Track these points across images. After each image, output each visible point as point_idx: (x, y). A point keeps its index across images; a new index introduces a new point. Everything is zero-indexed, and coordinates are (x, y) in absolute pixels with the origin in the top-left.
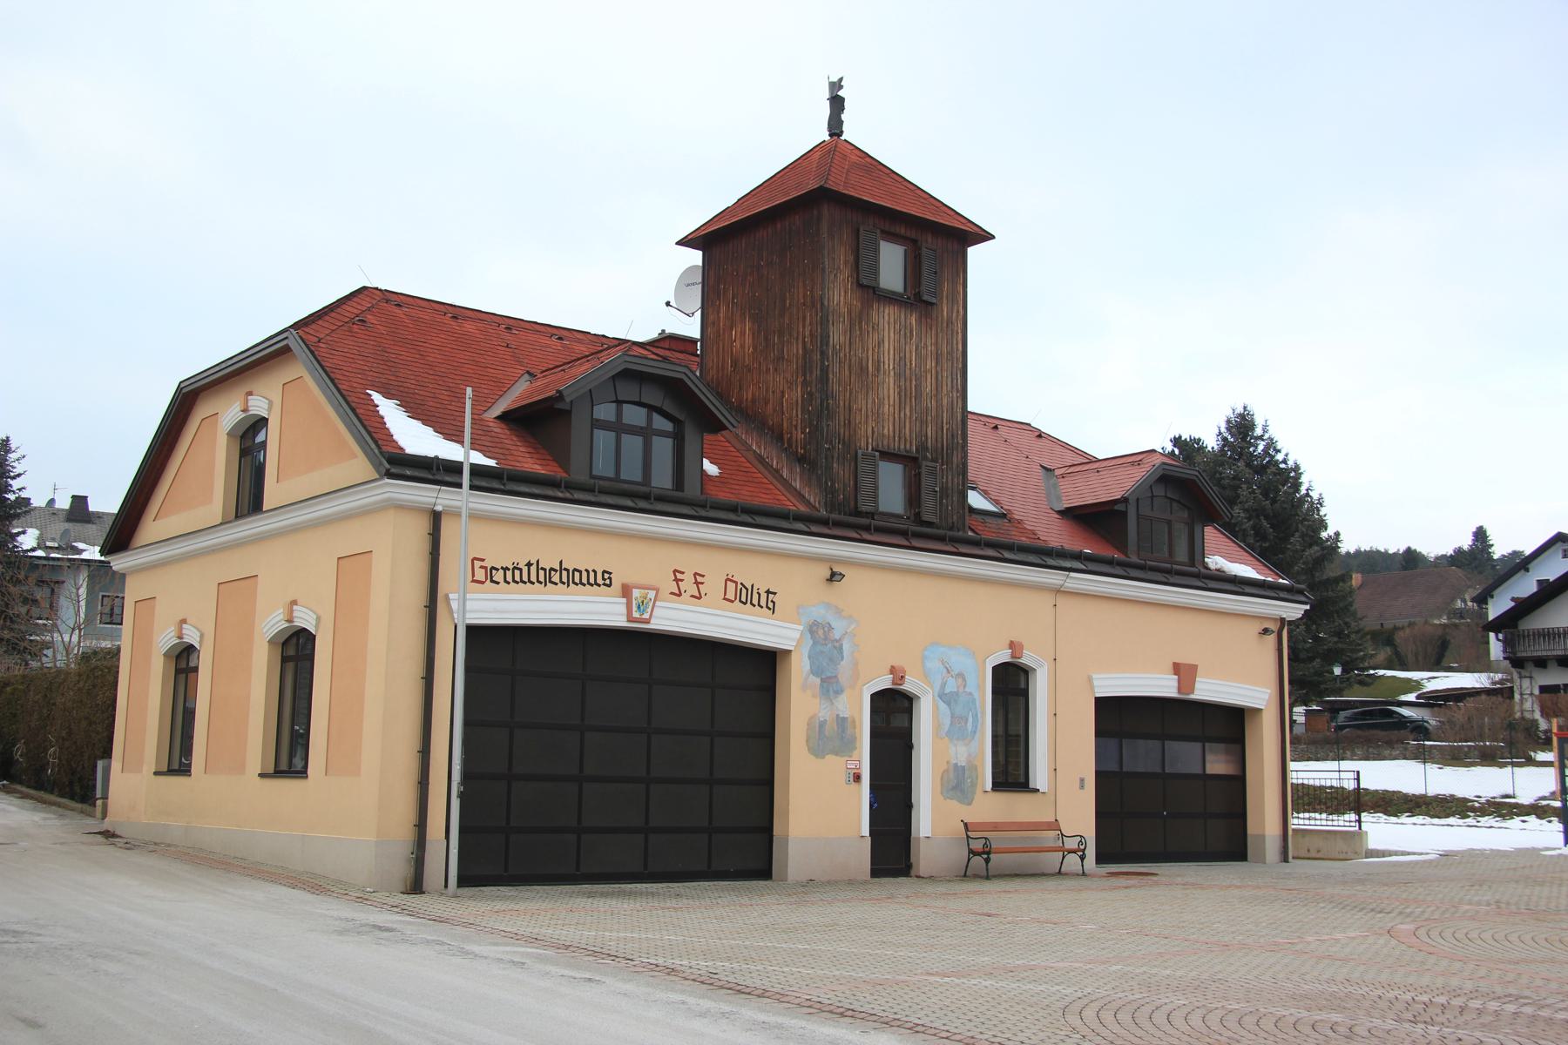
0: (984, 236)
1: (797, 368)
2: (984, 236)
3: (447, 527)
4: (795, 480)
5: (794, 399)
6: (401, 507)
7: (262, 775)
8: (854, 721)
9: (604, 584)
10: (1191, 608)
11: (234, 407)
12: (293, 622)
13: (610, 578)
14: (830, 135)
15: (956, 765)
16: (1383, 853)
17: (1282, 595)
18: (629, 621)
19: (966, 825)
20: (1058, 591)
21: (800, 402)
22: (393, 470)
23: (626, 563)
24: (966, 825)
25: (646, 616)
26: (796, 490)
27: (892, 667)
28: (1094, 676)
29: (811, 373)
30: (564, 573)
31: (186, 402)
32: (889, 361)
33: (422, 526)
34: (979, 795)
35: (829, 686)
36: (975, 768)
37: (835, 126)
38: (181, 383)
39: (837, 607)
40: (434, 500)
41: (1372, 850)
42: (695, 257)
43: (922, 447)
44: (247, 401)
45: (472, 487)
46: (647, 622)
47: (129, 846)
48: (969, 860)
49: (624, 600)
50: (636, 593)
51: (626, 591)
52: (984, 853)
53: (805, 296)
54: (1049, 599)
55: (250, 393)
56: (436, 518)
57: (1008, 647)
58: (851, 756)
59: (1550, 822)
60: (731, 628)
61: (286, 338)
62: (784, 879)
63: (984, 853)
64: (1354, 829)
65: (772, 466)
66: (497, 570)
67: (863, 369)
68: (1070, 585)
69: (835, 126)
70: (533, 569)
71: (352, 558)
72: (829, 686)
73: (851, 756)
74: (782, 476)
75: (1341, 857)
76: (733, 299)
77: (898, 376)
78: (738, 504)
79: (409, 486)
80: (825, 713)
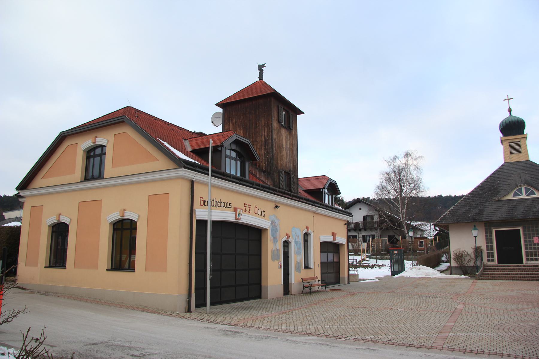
0: (302, 113)
1: (262, 144)
2: (302, 113)
3: (196, 186)
4: (262, 178)
5: (261, 153)
6: (182, 178)
7: (107, 270)
8: (280, 250)
9: (230, 207)
10: (325, 216)
11: (89, 141)
12: (124, 217)
13: (231, 205)
14: (259, 80)
15: (298, 262)
16: (364, 280)
17: (340, 212)
18: (236, 219)
19: (302, 279)
20: (315, 213)
21: (263, 154)
22: (186, 166)
23: (237, 201)
24: (302, 279)
25: (240, 218)
26: (262, 180)
27: (287, 234)
28: (321, 236)
29: (268, 146)
30: (221, 203)
31: (62, 138)
32: (284, 144)
33: (188, 185)
34: (302, 270)
35: (275, 240)
36: (301, 262)
37: (261, 77)
38: (61, 132)
39: (276, 216)
40: (193, 177)
41: (360, 279)
42: (221, 110)
43: (290, 170)
44: (96, 139)
45: (213, 176)
46: (240, 220)
47: (31, 292)
48: (303, 289)
49: (235, 213)
50: (238, 210)
51: (235, 210)
52: (309, 287)
53: (265, 123)
54: (312, 215)
55: (96, 137)
56: (192, 183)
57: (306, 228)
58: (279, 261)
59: (365, 269)
60: (249, 220)
61: (123, 118)
62: (266, 298)
63: (309, 287)
64: (355, 274)
65: (252, 173)
66: (206, 201)
67: (280, 146)
68: (318, 211)
69: (261, 77)
70: (214, 201)
71: (156, 195)
72: (275, 240)
73: (279, 261)
74: (256, 176)
75: (352, 281)
76: (235, 122)
77: (286, 149)
78: (260, 184)
79: (189, 171)
80: (274, 249)
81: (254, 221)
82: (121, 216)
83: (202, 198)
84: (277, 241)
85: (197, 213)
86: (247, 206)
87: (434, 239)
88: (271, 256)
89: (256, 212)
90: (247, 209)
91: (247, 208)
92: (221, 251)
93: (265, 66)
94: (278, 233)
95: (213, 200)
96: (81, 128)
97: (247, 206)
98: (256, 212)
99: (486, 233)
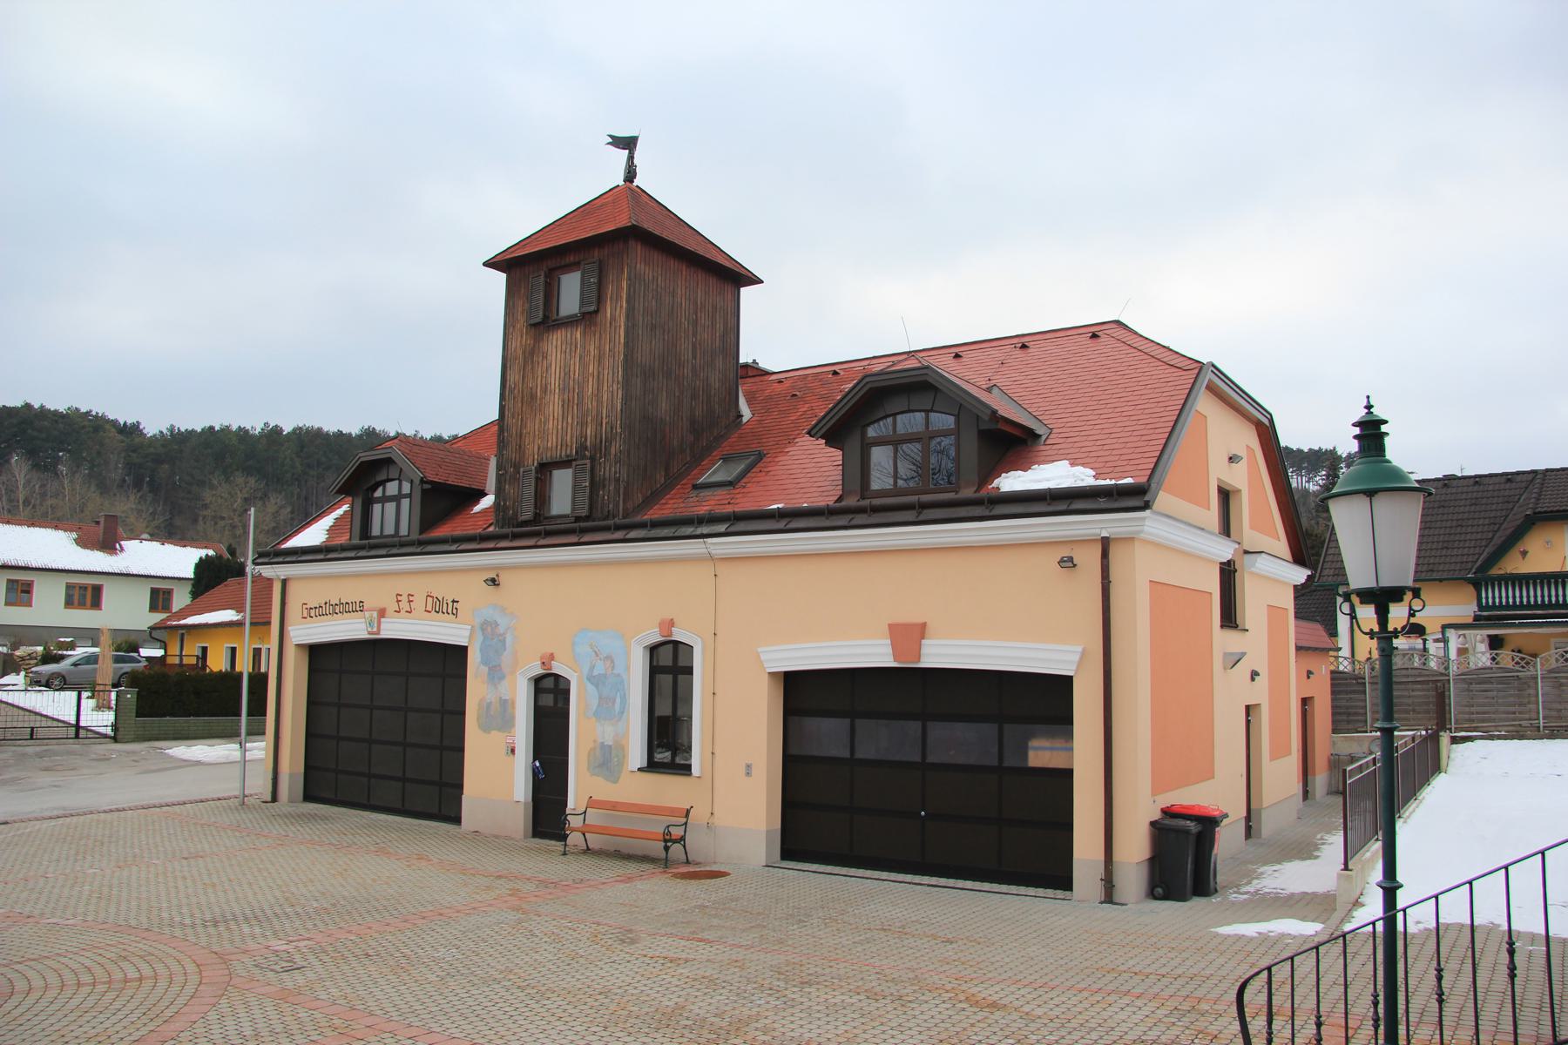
37: (630, 174)
81: (419, 632)
82: (369, 633)
83: (306, 604)
84: (502, 678)
85: (292, 634)
86: (404, 599)
87: (1445, 724)
88: (478, 719)
89: (429, 608)
90: (404, 605)
91: (404, 605)
92: (339, 700)
93: (610, 136)
94: (505, 653)
95: (326, 603)
96: (830, 415)
97: (404, 599)
98: (429, 608)
99: (543, 693)
